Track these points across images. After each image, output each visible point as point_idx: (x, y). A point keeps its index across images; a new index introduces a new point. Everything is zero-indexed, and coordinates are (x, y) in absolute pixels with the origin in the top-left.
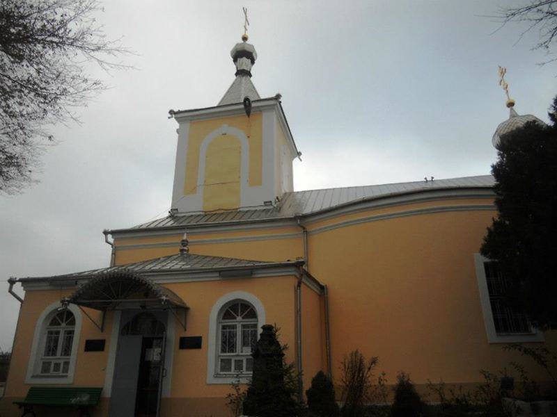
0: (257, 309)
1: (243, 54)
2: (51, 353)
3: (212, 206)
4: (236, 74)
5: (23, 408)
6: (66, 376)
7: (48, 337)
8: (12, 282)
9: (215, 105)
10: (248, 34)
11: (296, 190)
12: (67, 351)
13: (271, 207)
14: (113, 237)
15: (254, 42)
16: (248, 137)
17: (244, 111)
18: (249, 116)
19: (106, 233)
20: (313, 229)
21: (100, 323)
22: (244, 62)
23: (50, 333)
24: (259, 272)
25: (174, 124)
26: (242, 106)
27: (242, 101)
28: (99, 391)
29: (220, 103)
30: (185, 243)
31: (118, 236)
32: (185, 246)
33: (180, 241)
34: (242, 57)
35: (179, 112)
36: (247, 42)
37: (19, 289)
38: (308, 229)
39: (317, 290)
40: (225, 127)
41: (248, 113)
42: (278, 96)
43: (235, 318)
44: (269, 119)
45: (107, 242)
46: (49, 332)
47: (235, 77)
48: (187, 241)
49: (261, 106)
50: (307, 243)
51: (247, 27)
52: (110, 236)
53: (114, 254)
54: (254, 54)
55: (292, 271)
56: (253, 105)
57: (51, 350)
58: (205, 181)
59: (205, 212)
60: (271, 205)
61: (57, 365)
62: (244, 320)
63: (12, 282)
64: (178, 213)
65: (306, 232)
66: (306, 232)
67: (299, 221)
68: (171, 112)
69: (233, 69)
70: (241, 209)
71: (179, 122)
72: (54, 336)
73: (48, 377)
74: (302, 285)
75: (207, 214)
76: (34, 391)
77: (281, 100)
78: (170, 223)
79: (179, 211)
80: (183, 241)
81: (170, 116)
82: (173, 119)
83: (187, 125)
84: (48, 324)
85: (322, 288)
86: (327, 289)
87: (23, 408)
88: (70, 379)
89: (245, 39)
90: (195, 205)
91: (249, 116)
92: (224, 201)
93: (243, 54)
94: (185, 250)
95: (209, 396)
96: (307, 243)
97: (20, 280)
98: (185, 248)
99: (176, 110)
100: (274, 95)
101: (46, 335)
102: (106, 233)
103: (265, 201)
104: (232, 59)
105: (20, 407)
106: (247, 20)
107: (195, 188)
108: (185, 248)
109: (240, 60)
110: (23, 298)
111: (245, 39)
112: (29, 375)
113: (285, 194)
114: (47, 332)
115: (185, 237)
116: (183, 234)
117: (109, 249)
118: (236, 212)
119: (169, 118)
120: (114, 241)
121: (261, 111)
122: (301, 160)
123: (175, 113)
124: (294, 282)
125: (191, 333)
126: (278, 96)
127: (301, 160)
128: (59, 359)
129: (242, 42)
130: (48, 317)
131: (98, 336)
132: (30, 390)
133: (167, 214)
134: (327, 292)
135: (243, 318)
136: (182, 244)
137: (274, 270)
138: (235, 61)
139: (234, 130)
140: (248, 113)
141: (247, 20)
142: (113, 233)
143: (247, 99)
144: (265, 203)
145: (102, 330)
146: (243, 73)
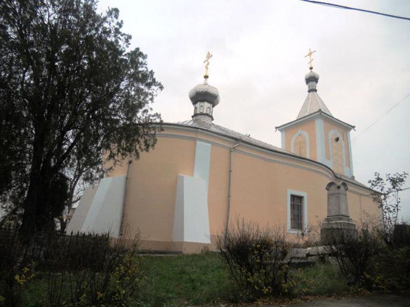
22: (311, 83)
25: (279, 133)
68: (276, 128)
69: (306, 88)
99: (278, 126)
138: (307, 84)
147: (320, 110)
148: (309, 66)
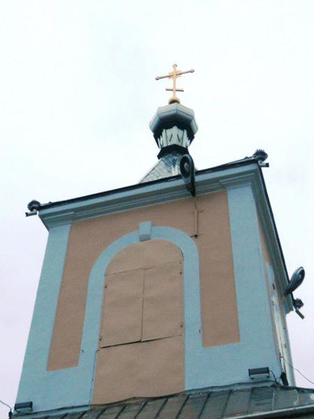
0: (144, 233)
4: (159, 156)
22: (173, 135)
41: (193, 193)
42: (261, 155)
44: (240, 202)
47: (157, 160)
54: (193, 123)
68: (34, 207)
81: (29, 211)
82: (36, 219)
83: (65, 231)
99: (43, 202)
100: (250, 153)
104: (152, 134)
109: (167, 133)
119: (27, 215)
122: (302, 317)
123: (40, 208)
126: (261, 155)
127: (302, 317)
140: (193, 193)
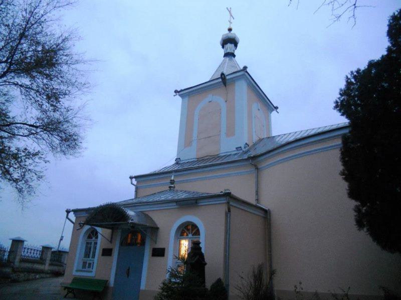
1: (230, 41)
2: (87, 256)
3: (203, 153)
5: (67, 289)
6: (91, 272)
7: (86, 246)
8: (68, 212)
9: (208, 80)
10: (232, 27)
11: (274, 133)
12: (94, 256)
13: (242, 151)
14: (136, 180)
15: (237, 33)
16: (226, 101)
17: (222, 83)
18: (225, 86)
19: (131, 178)
20: (263, 166)
21: (110, 239)
22: (230, 47)
23: (87, 243)
24: (202, 201)
25: (179, 99)
26: (220, 80)
27: (220, 76)
28: (106, 282)
29: (212, 78)
30: (172, 182)
31: (139, 179)
32: (172, 184)
33: (169, 181)
34: (227, 44)
35: (182, 91)
36: (232, 32)
37: (72, 216)
38: (259, 167)
39: (261, 214)
40: (210, 97)
42: (245, 68)
43: (92, 238)
45: (132, 183)
46: (87, 243)
48: (174, 181)
49: (234, 77)
50: (257, 177)
51: (232, 20)
52: (134, 180)
53: (136, 191)
55: (223, 200)
56: (227, 78)
57: (87, 255)
58: (198, 137)
59: (198, 158)
60: (241, 149)
61: (90, 264)
62: (193, 237)
63: (68, 212)
64: (180, 161)
65: (257, 169)
66: (257, 169)
67: (251, 161)
68: (176, 92)
69: (222, 52)
70: (220, 155)
71: (181, 97)
72: (89, 245)
73: (84, 271)
74: (232, 209)
75: (199, 160)
76: (76, 280)
77: (248, 70)
78: (135, 201)
79: (181, 159)
80: (171, 180)
81: (175, 94)
83: (186, 99)
84: (86, 238)
85: (266, 212)
86: (270, 213)
87: (67, 289)
88: (91, 274)
89: (230, 30)
90: (192, 154)
91: (225, 86)
92: (210, 150)
93: (230, 41)
94: (172, 187)
95: (309, 291)
96: (257, 177)
97: (73, 211)
98: (173, 186)
99: (179, 90)
101: (85, 245)
102: (131, 178)
103: (237, 147)
104: (221, 47)
105: (65, 289)
106: (231, 15)
107: (191, 142)
108: (173, 186)
110: (74, 221)
111: (230, 30)
112: (75, 269)
113: (261, 140)
114: (85, 242)
115: (172, 178)
116: (171, 176)
117: (134, 188)
118: (217, 157)
120: (137, 183)
121: (234, 81)
122: (278, 113)
123: (179, 92)
124: (224, 208)
125: (159, 245)
127: (278, 113)
128: (90, 260)
129: (228, 32)
130: (84, 236)
131: (109, 246)
132: (73, 279)
133: (174, 162)
134: (270, 216)
135: (193, 235)
136: (171, 183)
137: (216, 199)
138: (223, 47)
139: (217, 98)
141: (231, 15)
142: (136, 177)
143: (222, 74)
144: (237, 148)
145: (111, 242)
146: (230, 55)
147: (188, 94)
148: (228, 27)
